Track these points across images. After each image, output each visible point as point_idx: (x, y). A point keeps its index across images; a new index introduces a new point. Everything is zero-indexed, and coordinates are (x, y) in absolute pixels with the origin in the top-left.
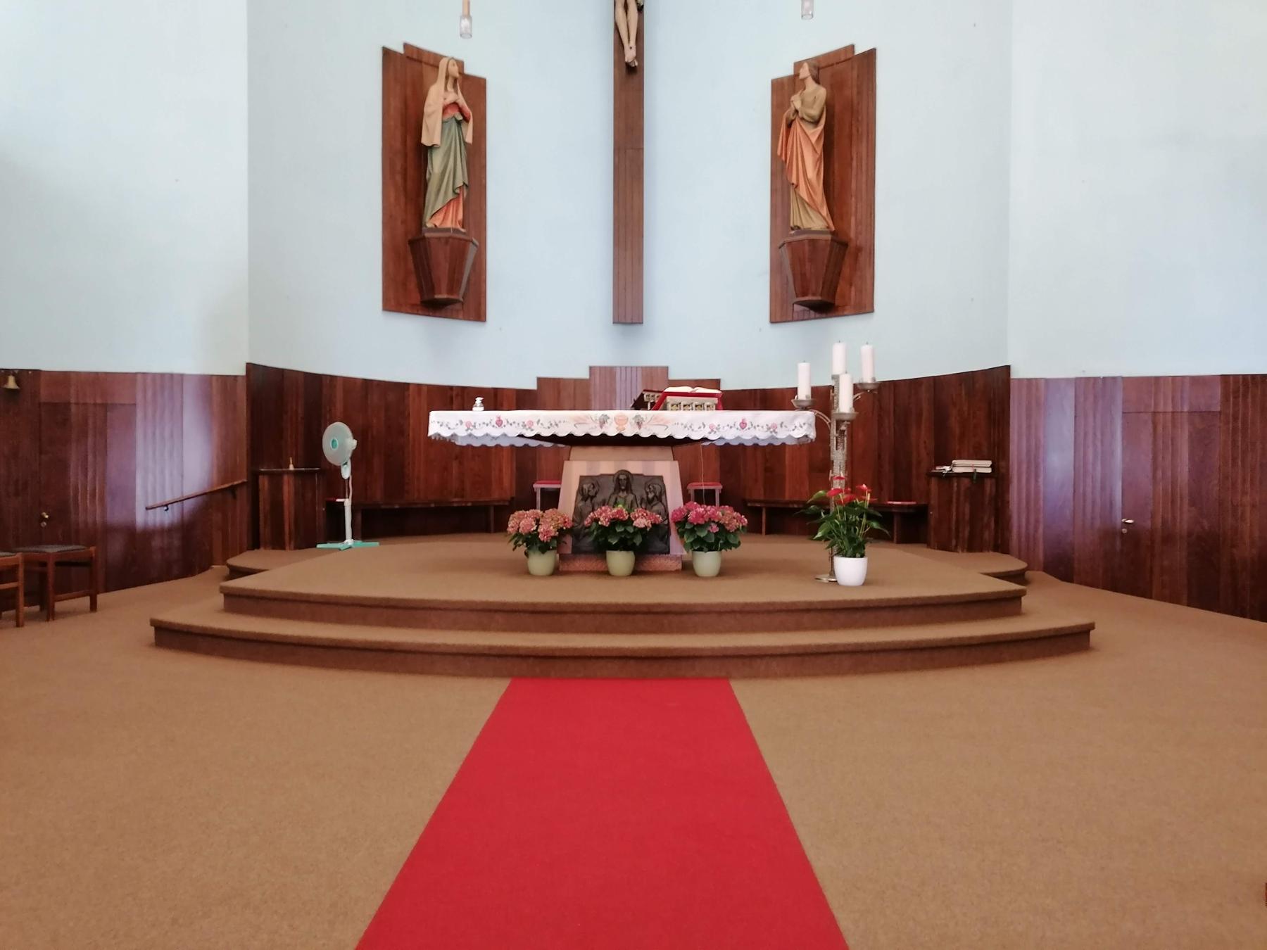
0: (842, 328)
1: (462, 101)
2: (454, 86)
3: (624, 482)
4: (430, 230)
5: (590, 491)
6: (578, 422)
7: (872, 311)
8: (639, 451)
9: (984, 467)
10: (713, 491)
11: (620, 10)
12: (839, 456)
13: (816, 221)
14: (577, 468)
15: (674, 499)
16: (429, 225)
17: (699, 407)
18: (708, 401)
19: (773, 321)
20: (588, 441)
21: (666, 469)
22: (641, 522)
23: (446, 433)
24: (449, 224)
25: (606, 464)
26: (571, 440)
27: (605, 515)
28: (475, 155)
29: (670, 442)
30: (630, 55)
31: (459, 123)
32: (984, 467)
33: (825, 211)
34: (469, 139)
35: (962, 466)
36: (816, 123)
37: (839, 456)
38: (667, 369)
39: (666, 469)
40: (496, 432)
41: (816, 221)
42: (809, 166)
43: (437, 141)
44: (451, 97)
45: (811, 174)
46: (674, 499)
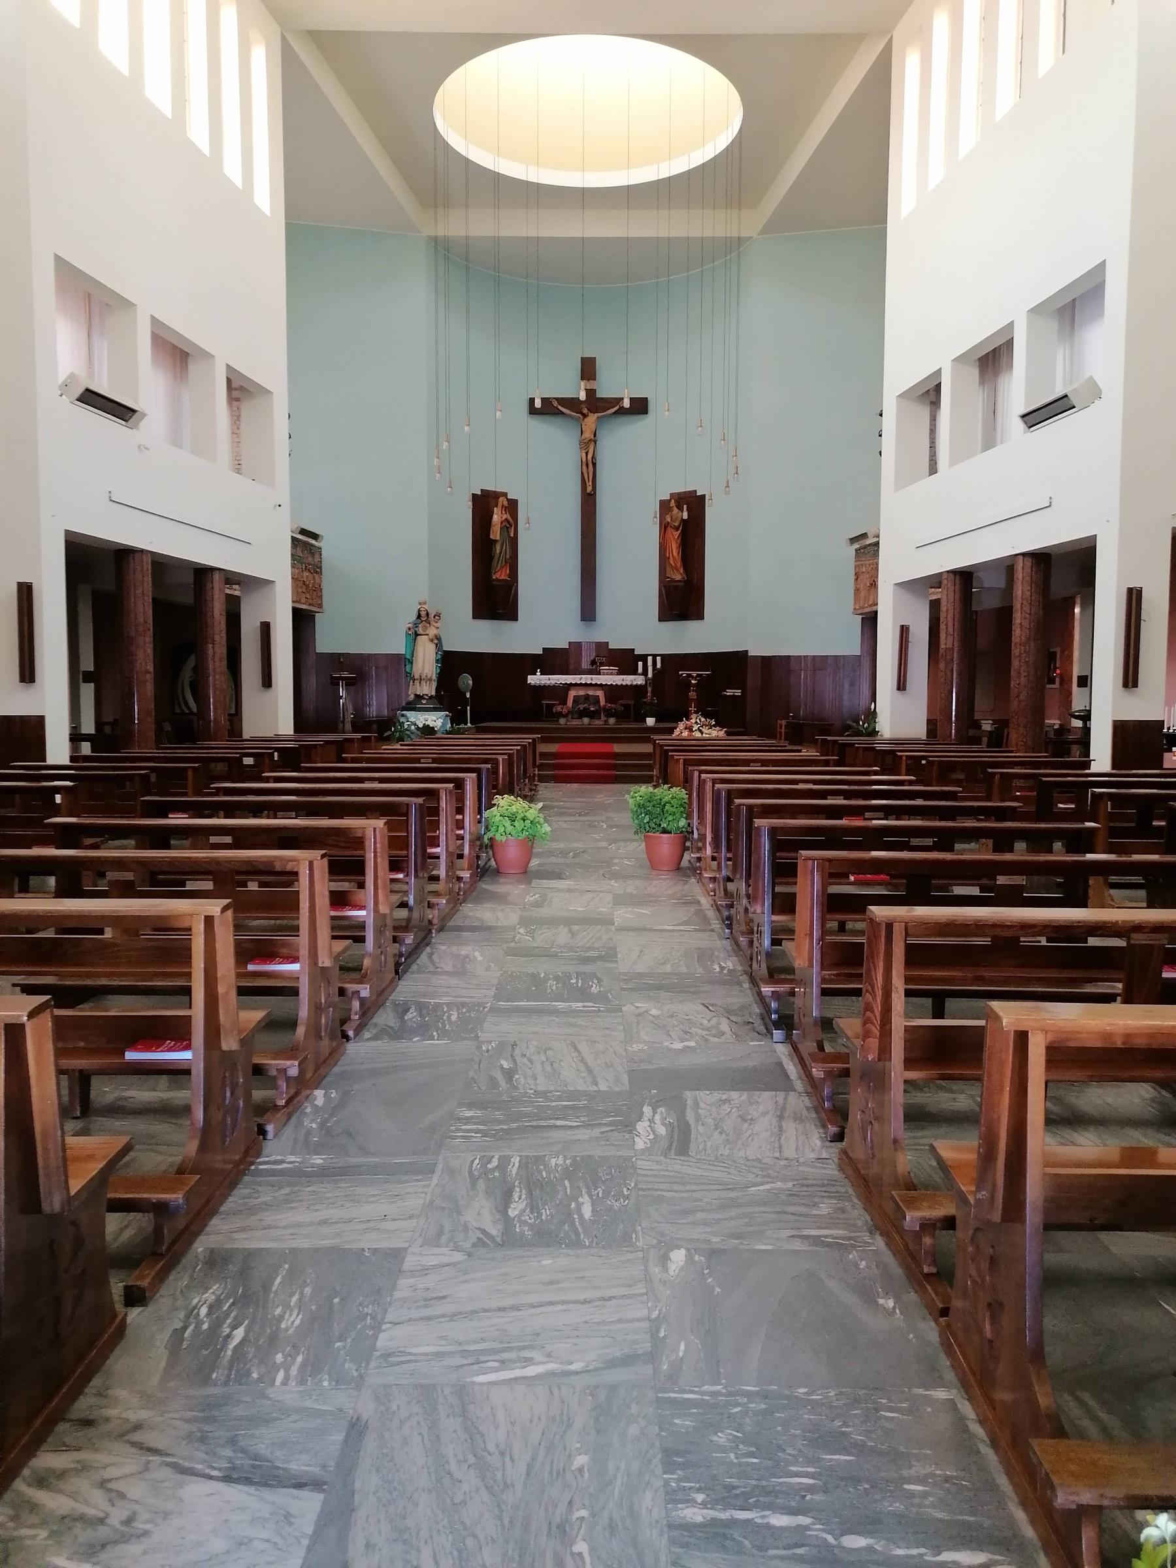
0: (691, 626)
1: (509, 518)
2: (505, 511)
3: (587, 697)
4: (495, 580)
5: (577, 700)
6: (573, 679)
7: (703, 619)
8: (592, 688)
9: (738, 693)
10: (629, 705)
11: (584, 467)
12: (649, 689)
13: (678, 576)
14: (572, 693)
15: (602, 702)
16: (494, 578)
17: (611, 674)
18: (614, 671)
19: (662, 618)
20: (576, 685)
21: (600, 693)
22: (592, 709)
23: (533, 682)
24: (503, 577)
25: (582, 693)
26: (571, 684)
27: (581, 707)
28: (514, 542)
29: (601, 685)
30: (589, 489)
31: (507, 528)
32: (738, 693)
33: (682, 571)
34: (512, 535)
35: (729, 692)
36: (677, 529)
37: (649, 689)
38: (696, 491)
39: (600, 693)
40: (548, 682)
41: (678, 576)
42: (674, 550)
43: (498, 538)
44: (505, 517)
45: (675, 553)
46: (602, 702)
